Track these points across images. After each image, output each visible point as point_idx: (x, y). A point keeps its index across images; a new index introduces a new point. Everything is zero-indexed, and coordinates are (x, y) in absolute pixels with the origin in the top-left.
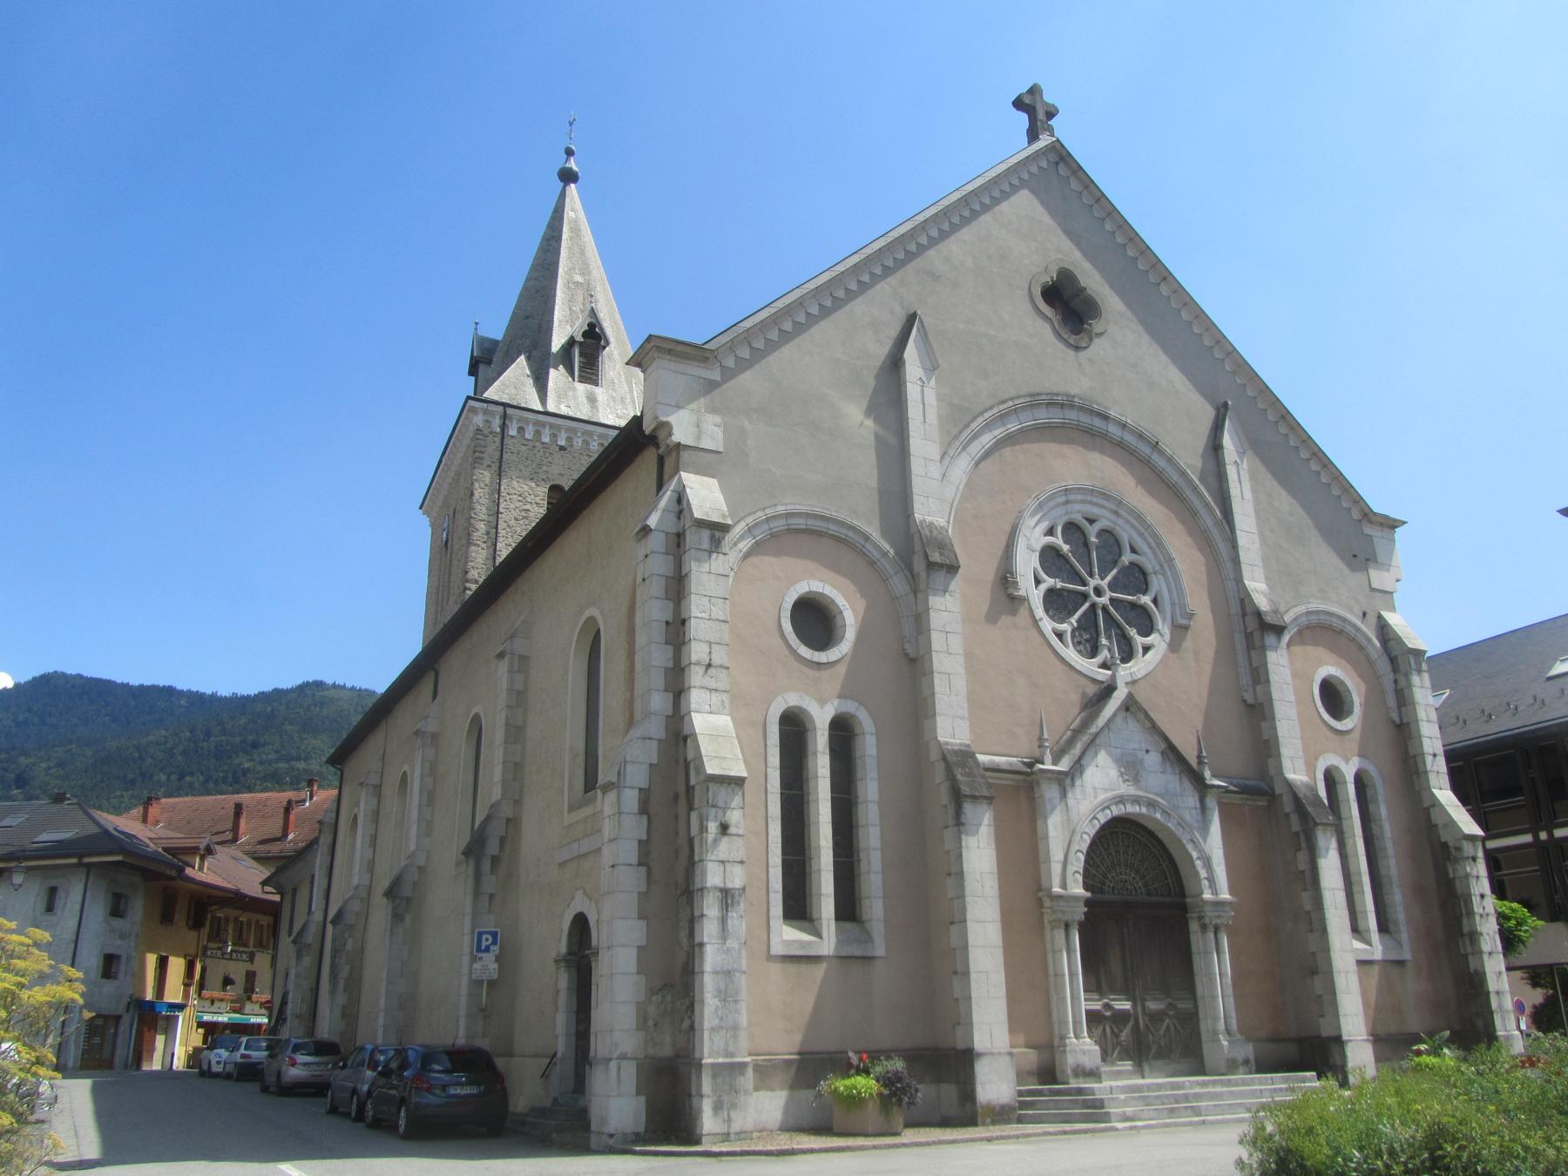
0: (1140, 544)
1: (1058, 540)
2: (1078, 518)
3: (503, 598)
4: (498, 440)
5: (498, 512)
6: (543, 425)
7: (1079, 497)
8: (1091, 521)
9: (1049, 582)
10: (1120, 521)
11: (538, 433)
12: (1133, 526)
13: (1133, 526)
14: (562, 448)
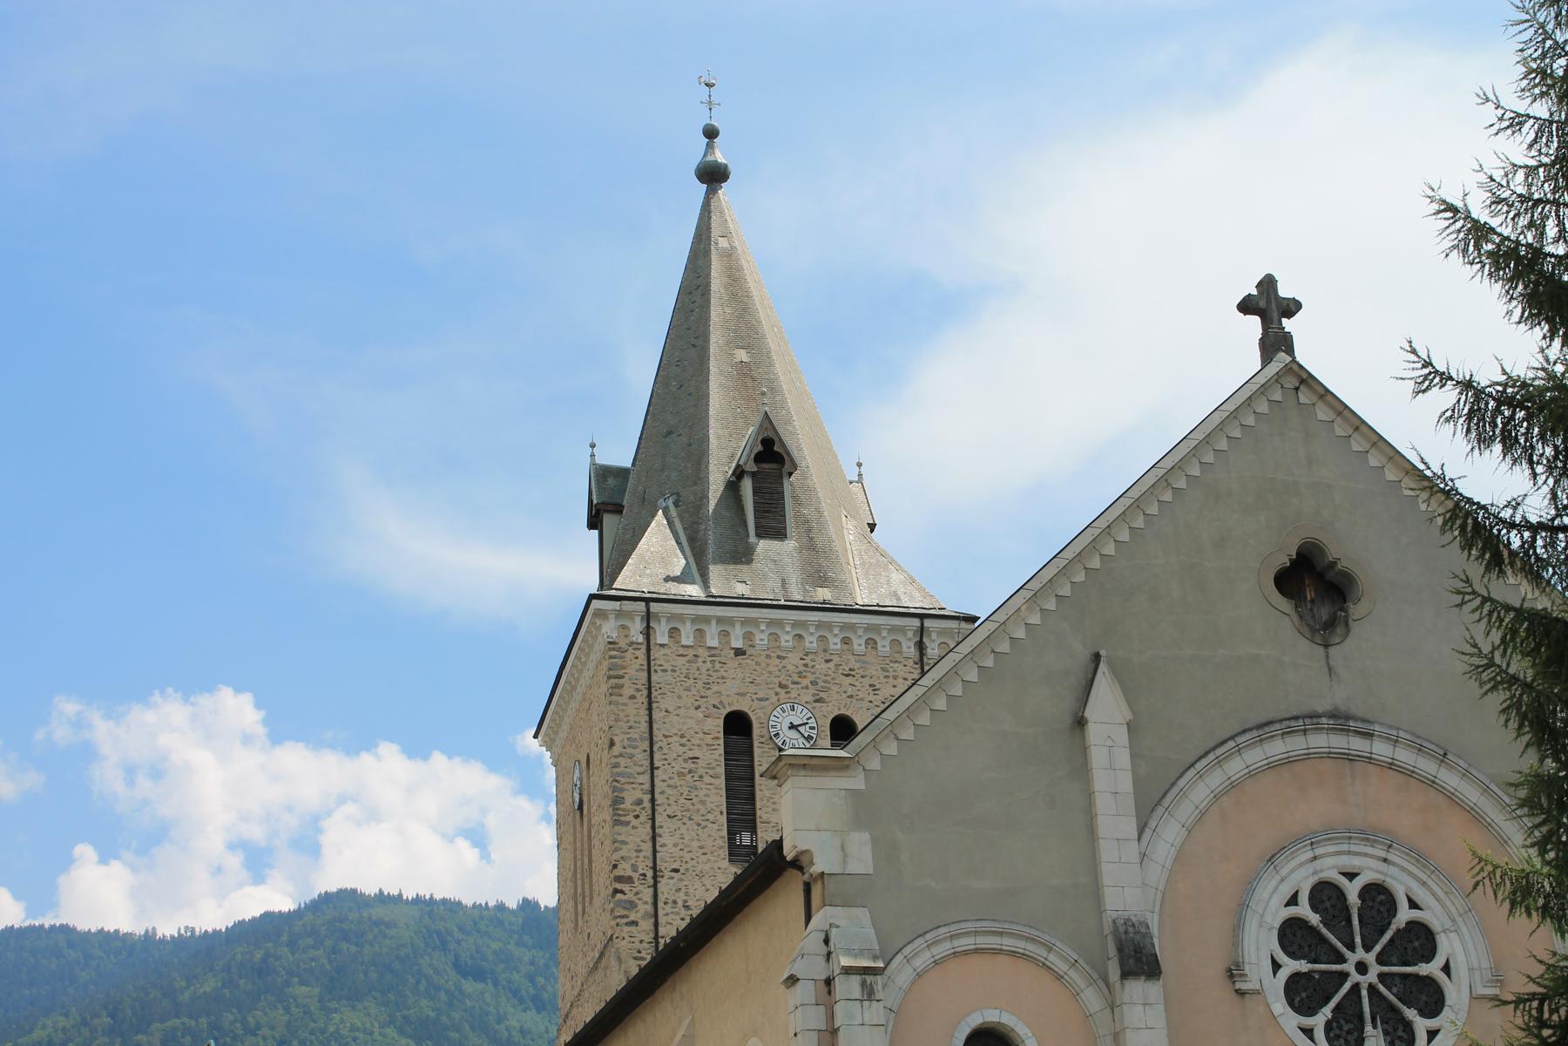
0: (1421, 895)
1: (1304, 910)
2: (1334, 876)
3: (658, 994)
4: (641, 653)
5: (653, 768)
6: (706, 620)
7: (1331, 849)
8: (1351, 876)
9: (1291, 966)
10: (1392, 870)
11: (700, 633)
12: (1411, 874)
13: (1411, 874)
14: (739, 652)
